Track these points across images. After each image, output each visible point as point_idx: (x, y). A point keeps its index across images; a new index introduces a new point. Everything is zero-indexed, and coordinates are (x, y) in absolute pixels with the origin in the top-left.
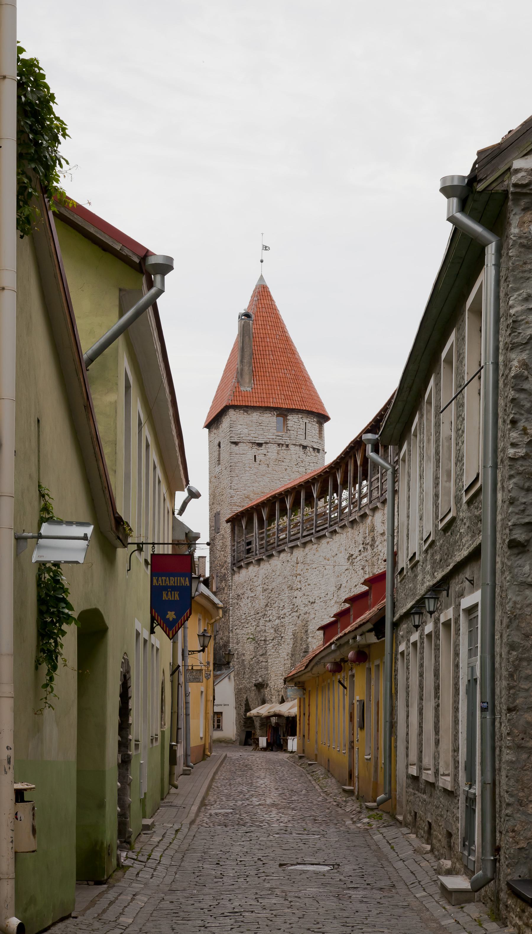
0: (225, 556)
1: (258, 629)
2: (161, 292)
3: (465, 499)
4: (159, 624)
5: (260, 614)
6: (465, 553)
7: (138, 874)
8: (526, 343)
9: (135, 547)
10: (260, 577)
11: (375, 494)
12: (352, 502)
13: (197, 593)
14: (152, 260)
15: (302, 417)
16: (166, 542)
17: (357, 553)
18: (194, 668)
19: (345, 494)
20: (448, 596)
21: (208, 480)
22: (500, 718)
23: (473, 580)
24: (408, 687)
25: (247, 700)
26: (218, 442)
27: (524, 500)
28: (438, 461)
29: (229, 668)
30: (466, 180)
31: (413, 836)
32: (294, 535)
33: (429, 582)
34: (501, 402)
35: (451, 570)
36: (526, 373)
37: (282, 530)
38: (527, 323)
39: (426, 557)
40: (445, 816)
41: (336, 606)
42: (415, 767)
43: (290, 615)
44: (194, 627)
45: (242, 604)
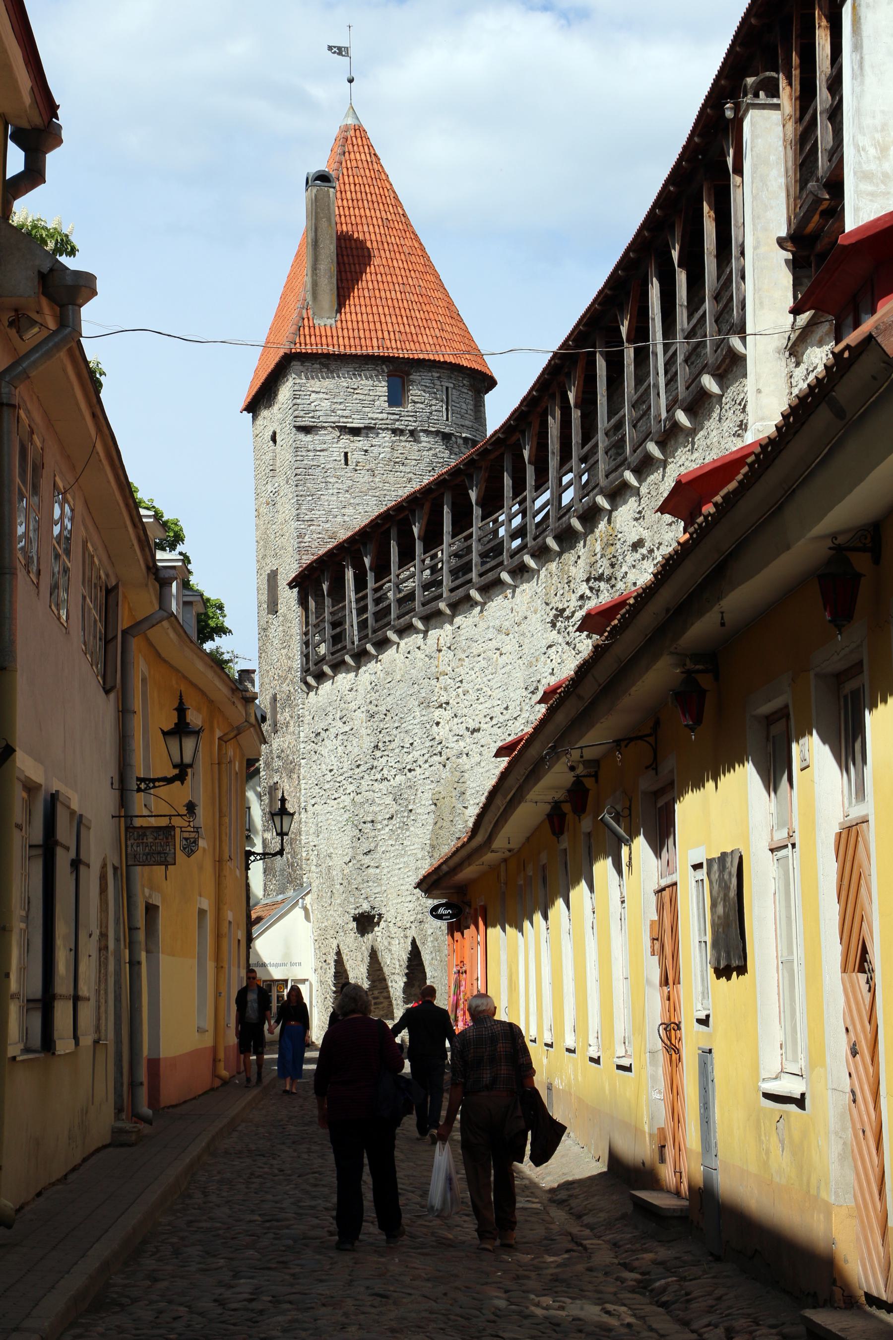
0: (289, 658)
1: (359, 799)
5: (362, 768)
10: (361, 691)
15: (439, 378)
17: (574, 603)
25: (339, 953)
26: (271, 433)
43: (426, 761)
45: (325, 752)
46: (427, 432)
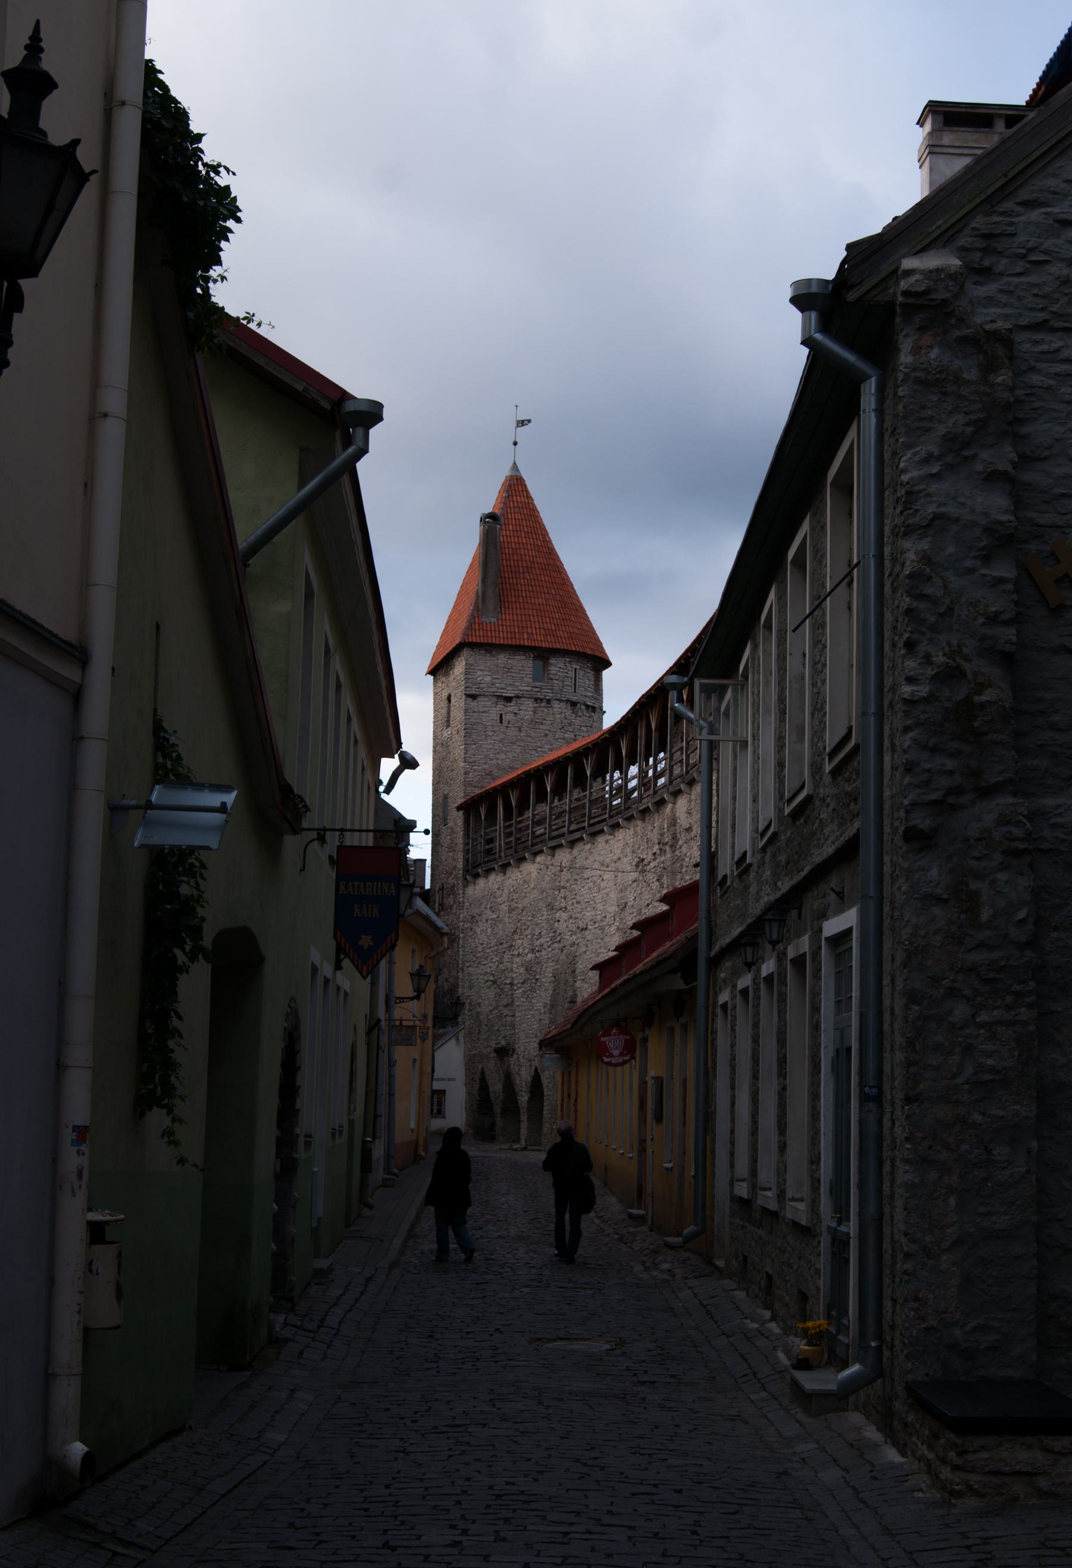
1: (502, 967)
2: (364, 451)
3: (828, 768)
4: (347, 956)
6: (829, 850)
7: (301, 1353)
8: (928, 526)
9: (314, 835)
11: (677, 771)
12: (644, 781)
13: (409, 911)
14: (350, 407)
16: (364, 828)
17: (650, 857)
18: (405, 1023)
19: (634, 770)
20: (800, 917)
21: (432, 749)
22: (892, 1113)
23: (843, 893)
24: (733, 1058)
25: (483, 1073)
27: (928, 766)
28: (783, 712)
29: (457, 1024)
30: (830, 287)
31: (741, 1295)
32: (557, 829)
33: (768, 896)
34: (888, 616)
35: (805, 877)
36: (928, 570)
37: (540, 823)
38: (928, 495)
39: (763, 858)
40: (796, 1267)
41: (617, 934)
42: (745, 1185)
44: (404, 960)
45: (478, 930)
46: (560, 700)
